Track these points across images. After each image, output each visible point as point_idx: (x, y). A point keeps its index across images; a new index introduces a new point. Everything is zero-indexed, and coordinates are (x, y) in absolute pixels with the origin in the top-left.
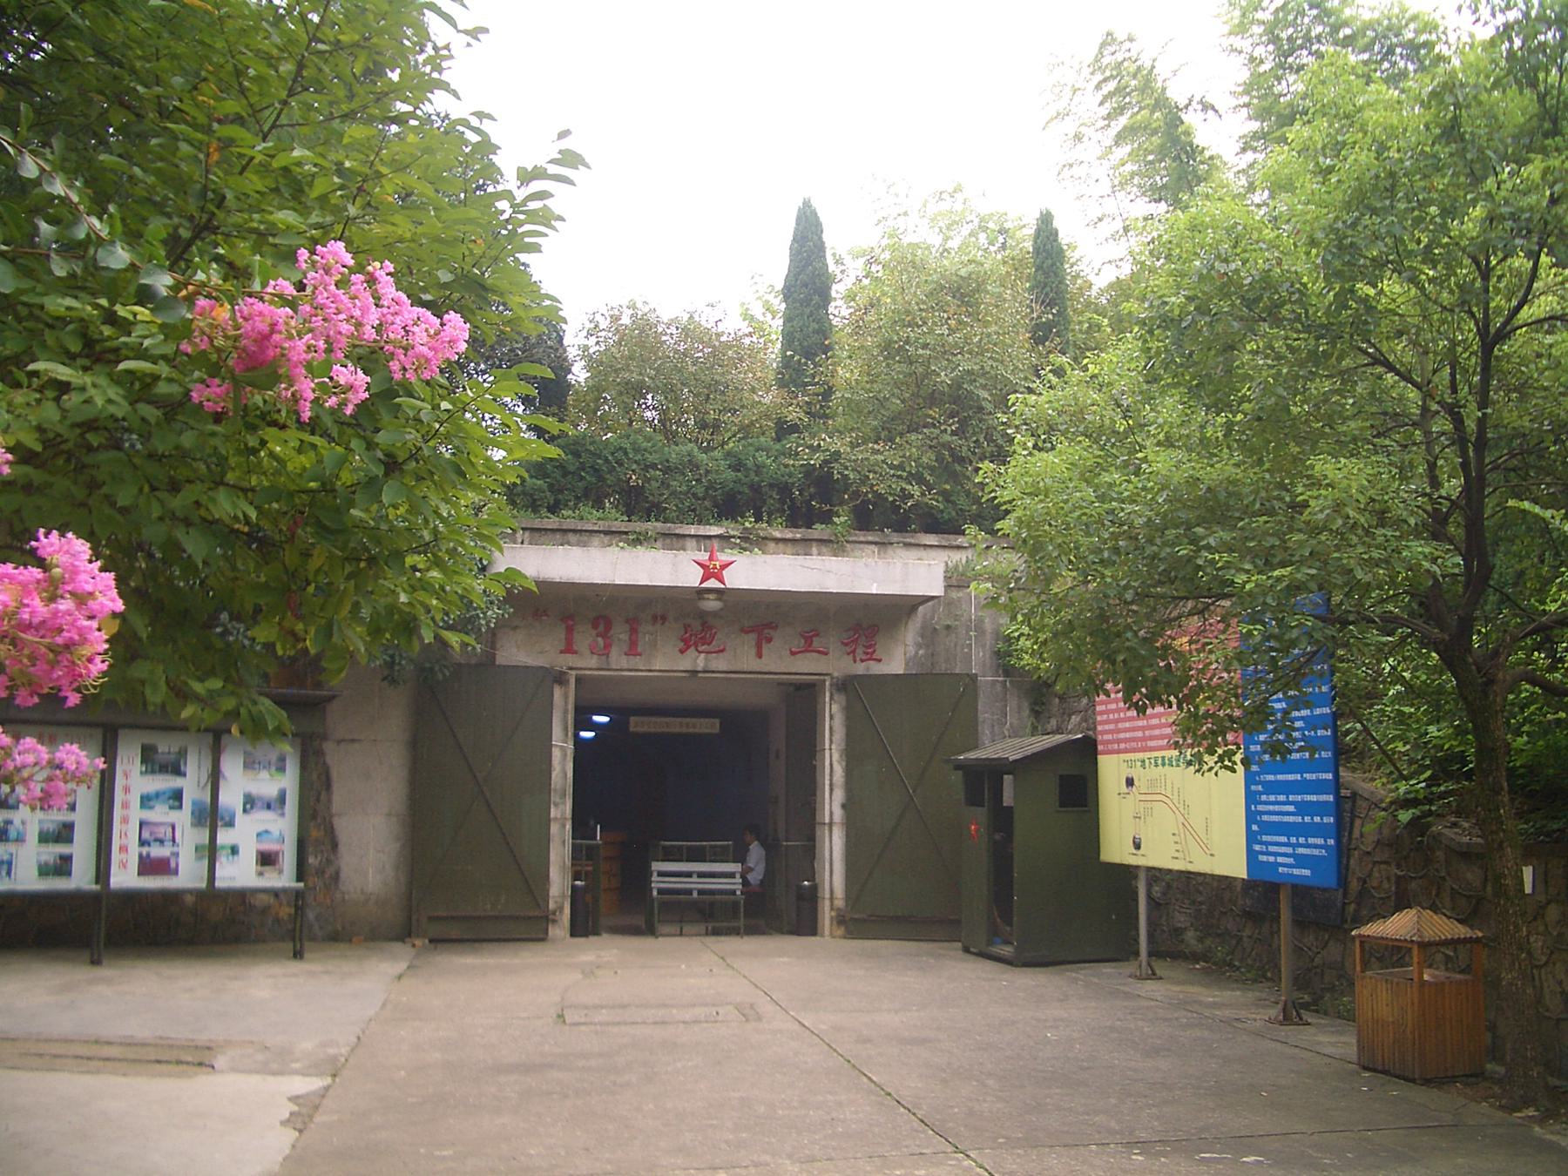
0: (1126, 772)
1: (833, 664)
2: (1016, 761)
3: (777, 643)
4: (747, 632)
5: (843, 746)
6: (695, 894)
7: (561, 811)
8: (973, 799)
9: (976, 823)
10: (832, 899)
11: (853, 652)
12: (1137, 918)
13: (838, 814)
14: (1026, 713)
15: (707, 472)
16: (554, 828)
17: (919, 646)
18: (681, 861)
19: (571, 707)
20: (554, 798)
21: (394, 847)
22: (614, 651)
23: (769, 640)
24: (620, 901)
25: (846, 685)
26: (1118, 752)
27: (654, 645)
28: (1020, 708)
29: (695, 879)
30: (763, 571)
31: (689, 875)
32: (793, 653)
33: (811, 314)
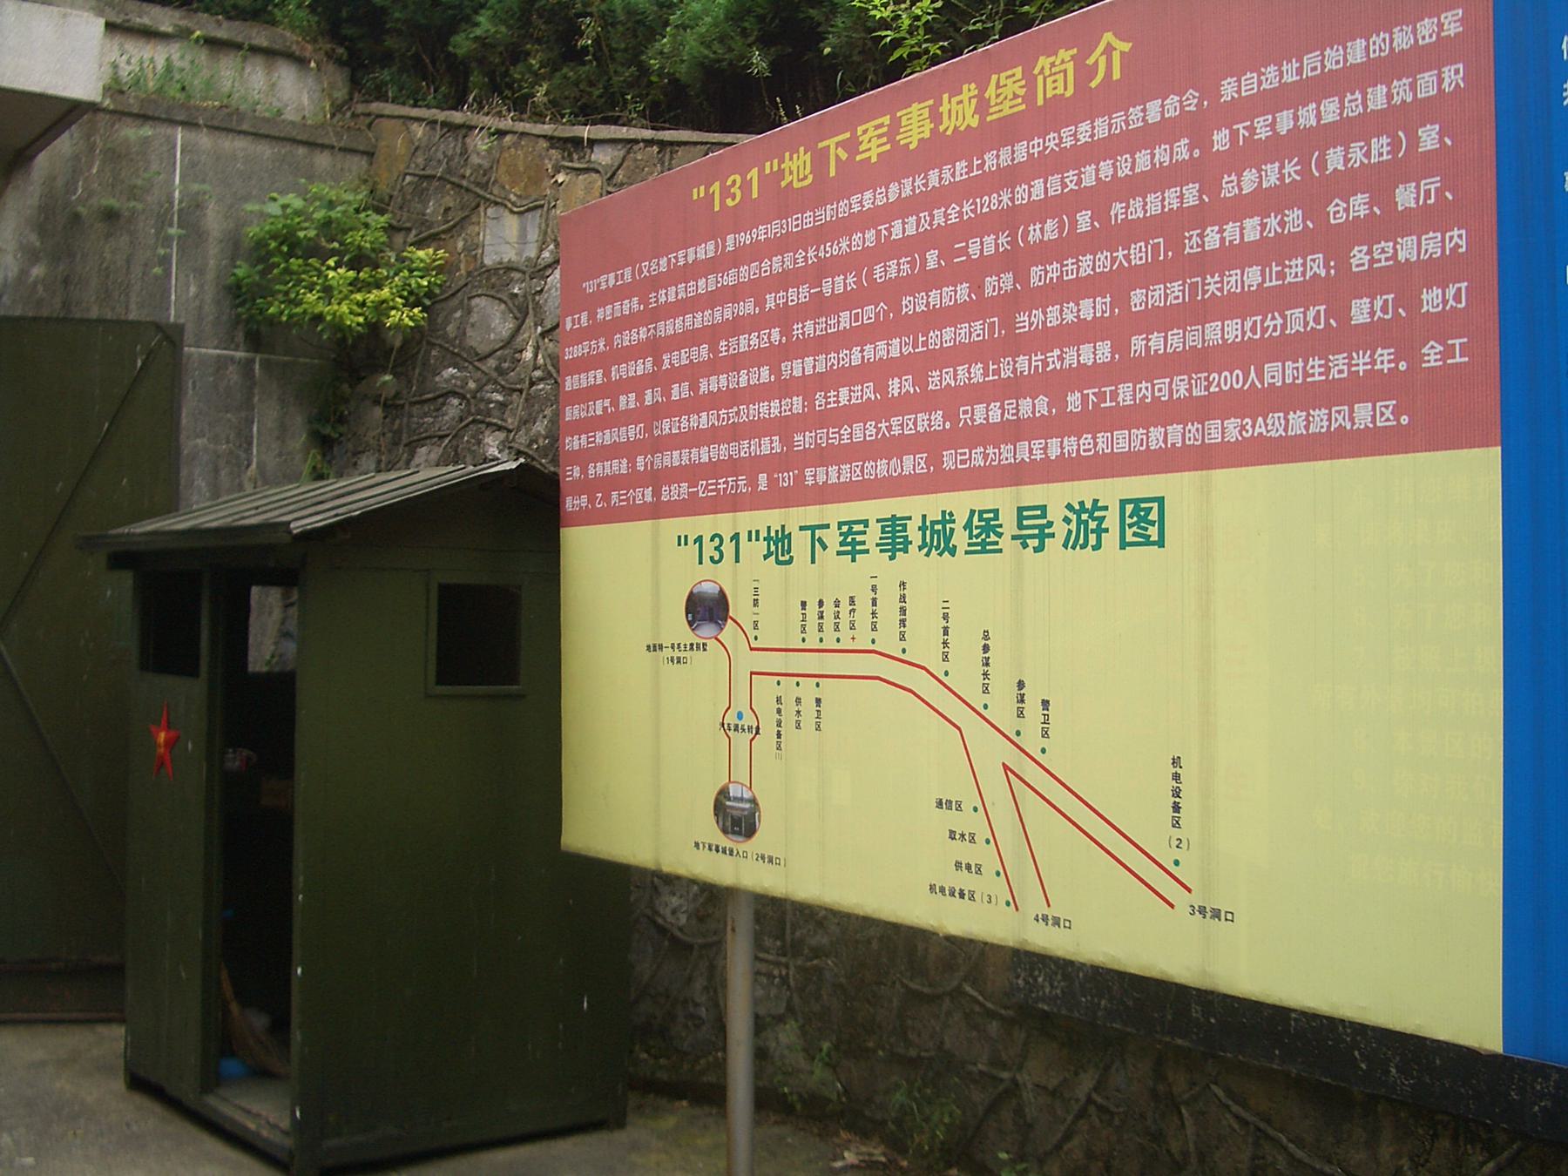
0: (687, 576)
2: (308, 536)
8: (166, 647)
9: (173, 723)
12: (198, 659)
14: (299, 440)
17: (32, 256)
26: (657, 511)
28: (283, 431)
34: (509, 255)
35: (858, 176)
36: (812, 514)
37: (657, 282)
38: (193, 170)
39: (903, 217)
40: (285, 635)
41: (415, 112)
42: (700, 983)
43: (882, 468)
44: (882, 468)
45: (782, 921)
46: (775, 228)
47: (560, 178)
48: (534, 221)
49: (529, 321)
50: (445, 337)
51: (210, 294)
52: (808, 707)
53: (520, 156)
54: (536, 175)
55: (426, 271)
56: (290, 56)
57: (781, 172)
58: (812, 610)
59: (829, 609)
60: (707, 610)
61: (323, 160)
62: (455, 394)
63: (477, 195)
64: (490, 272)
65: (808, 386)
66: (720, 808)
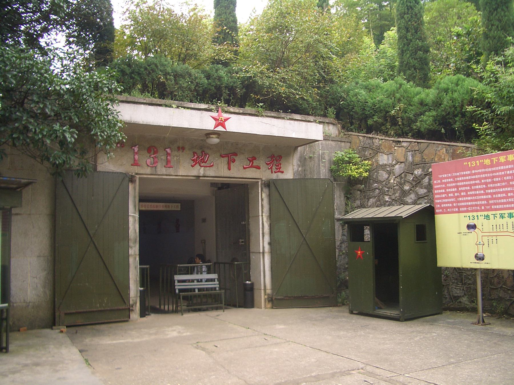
1: (264, 174)
3: (237, 163)
4: (223, 157)
5: (268, 214)
6: (197, 290)
7: (134, 250)
10: (265, 289)
11: (271, 168)
13: (267, 248)
14: (342, 199)
15: (196, 78)
16: (131, 260)
17: (299, 166)
18: (188, 274)
19: (137, 194)
20: (131, 244)
21: (43, 274)
22: (159, 165)
23: (234, 161)
24: (162, 296)
25: (268, 184)
26: (459, 212)
27: (178, 162)
28: (340, 196)
29: (196, 283)
30: (243, 124)
31: (193, 281)
32: (244, 168)
33: (230, 13)
34: (385, 162)
35: (499, 164)
36: (494, 212)
37: (457, 177)
38: (323, 149)
39: (509, 170)
40: (343, 235)
41: (360, 134)
42: (446, 291)
43: (508, 206)
44: (508, 206)
45: (487, 273)
46: (483, 170)
47: (396, 148)
48: (390, 157)
49: (392, 175)
50: (373, 178)
51: (327, 170)
52: (495, 241)
53: (387, 144)
54: (390, 148)
55: (368, 166)
56: (332, 123)
57: (484, 162)
58: (495, 226)
59: (498, 226)
60: (472, 227)
61: (343, 144)
62: (377, 189)
63: (377, 151)
64: (382, 166)
65: (491, 194)
66: (476, 256)
